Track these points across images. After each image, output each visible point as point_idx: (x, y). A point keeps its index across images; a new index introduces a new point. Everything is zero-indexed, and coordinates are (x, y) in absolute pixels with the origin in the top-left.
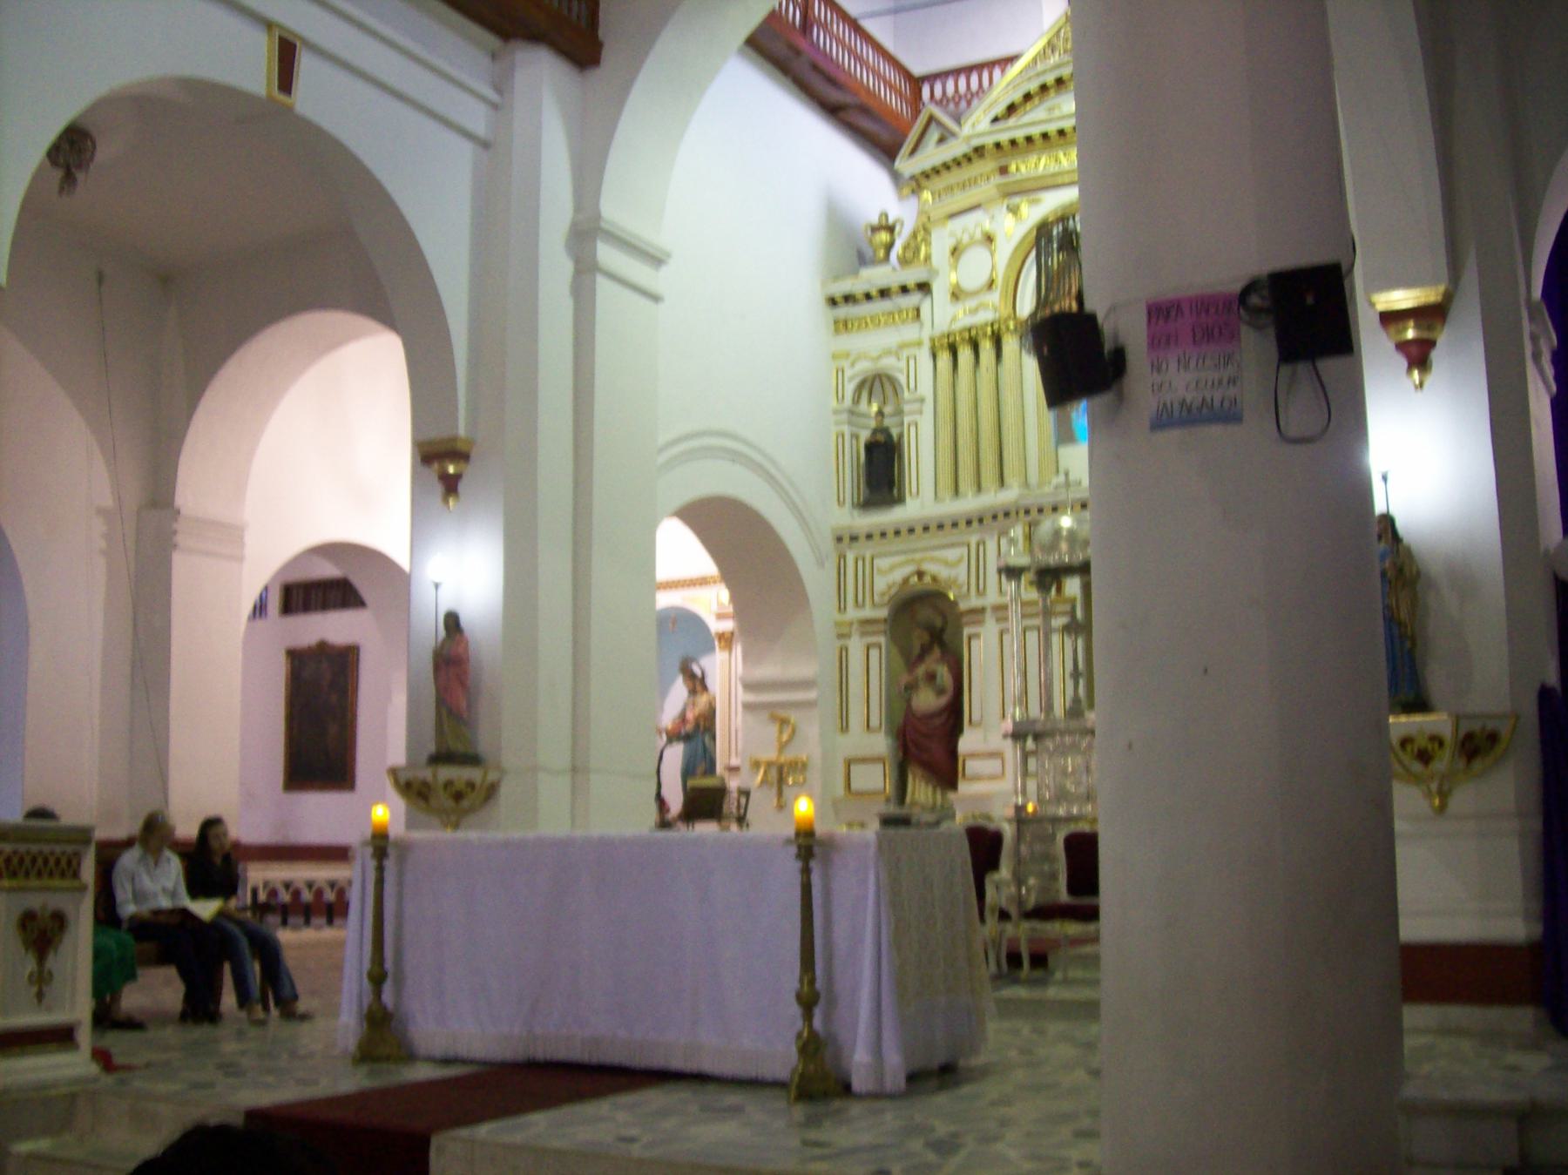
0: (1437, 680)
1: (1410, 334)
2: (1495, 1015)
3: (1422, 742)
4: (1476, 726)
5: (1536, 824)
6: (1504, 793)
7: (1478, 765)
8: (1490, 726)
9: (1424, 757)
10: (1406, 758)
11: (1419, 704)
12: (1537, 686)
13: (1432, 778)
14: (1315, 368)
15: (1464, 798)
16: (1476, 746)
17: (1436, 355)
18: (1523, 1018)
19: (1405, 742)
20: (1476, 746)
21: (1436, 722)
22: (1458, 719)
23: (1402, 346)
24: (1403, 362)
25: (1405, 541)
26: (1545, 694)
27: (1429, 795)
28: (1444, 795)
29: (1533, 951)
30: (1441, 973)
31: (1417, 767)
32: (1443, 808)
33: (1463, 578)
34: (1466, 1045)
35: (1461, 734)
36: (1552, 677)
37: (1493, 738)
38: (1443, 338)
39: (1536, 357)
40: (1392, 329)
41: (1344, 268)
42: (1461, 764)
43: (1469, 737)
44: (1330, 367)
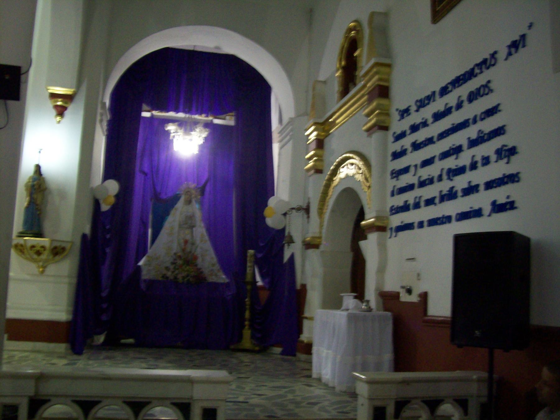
0: (47, 226)
1: (59, 103)
2: (52, 346)
3: (38, 248)
4: (58, 244)
5: (74, 281)
6: (65, 270)
7: (57, 258)
8: (64, 245)
9: (39, 253)
10: (32, 252)
11: (40, 235)
12: (81, 234)
13: (40, 261)
14: (6, 105)
15: (52, 269)
16: (57, 251)
17: (67, 113)
18: (62, 347)
19: (33, 247)
20: (57, 251)
21: (44, 241)
22: (52, 241)
23: (56, 107)
24: (54, 112)
25: (44, 176)
26: (84, 236)
27: (39, 267)
28: (44, 267)
29: (68, 324)
30: (25, 330)
31: (35, 256)
32: (43, 272)
33: (62, 194)
34: (40, 356)
35: (52, 247)
36: (87, 230)
37: (64, 249)
38: (71, 108)
39: (101, 121)
40: (53, 100)
41: (23, 71)
42: (51, 257)
43: (55, 248)
44: (11, 103)
